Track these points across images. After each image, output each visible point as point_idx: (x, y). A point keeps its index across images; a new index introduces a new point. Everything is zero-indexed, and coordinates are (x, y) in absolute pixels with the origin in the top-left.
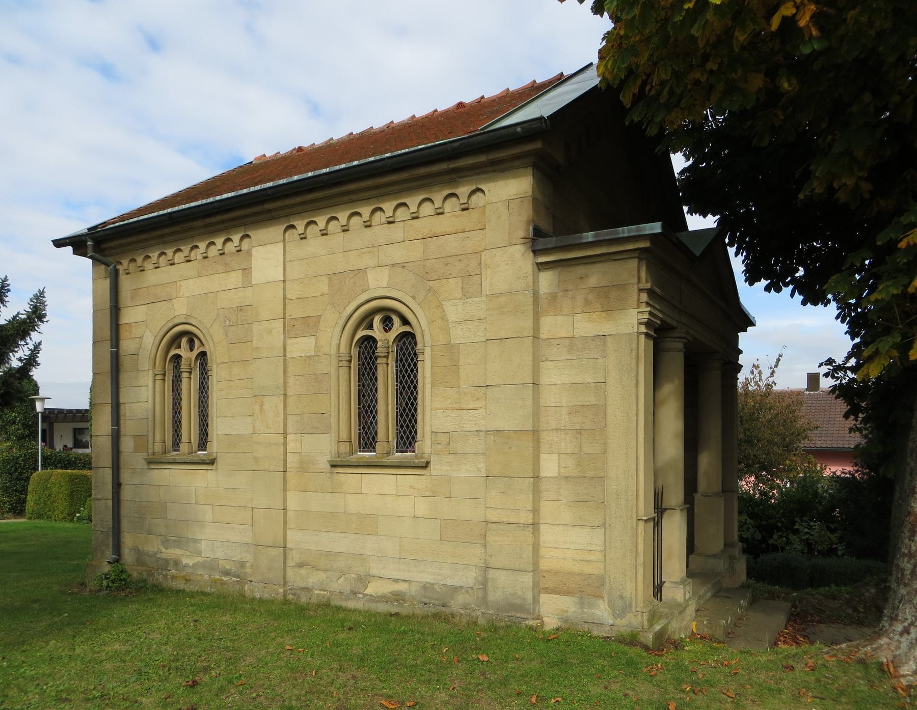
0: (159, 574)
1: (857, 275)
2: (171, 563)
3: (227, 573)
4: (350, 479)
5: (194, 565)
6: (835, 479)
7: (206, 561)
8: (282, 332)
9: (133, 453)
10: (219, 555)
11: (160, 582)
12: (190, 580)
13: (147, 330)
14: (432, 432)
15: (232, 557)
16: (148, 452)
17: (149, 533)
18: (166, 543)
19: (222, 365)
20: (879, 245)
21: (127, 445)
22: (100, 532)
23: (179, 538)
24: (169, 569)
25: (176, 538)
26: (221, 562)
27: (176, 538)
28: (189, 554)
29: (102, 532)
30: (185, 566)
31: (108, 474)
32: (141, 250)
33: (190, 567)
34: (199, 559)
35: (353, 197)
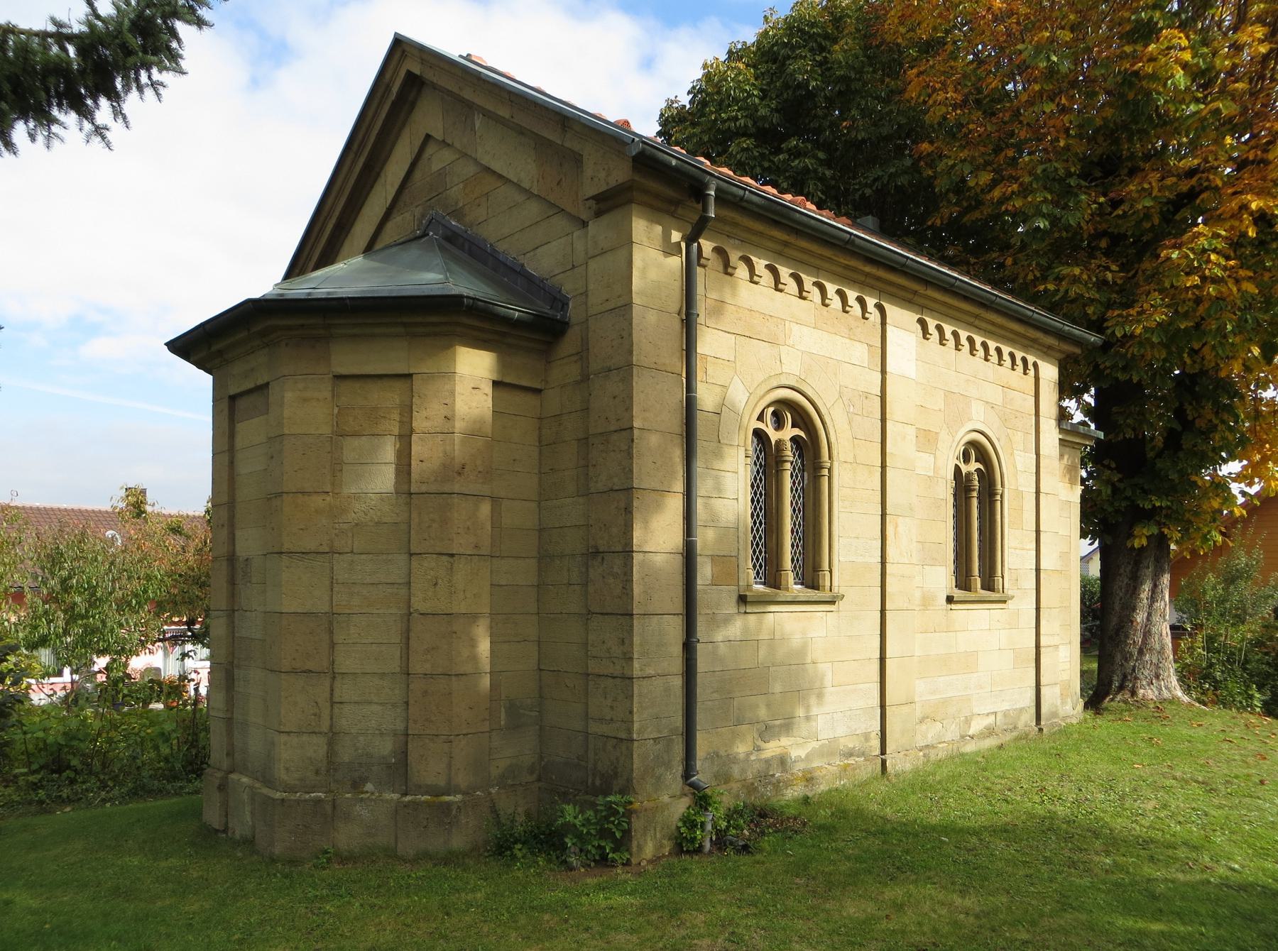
0: (765, 786)
1: (1228, 137)
2: (775, 764)
3: (850, 754)
4: (961, 614)
5: (807, 756)
6: (757, 591)
7: (823, 744)
8: (533, 130)
9: (709, 587)
10: (841, 731)
11: (769, 799)
12: (812, 778)
13: (736, 377)
14: (737, 473)
15: (856, 730)
16: (738, 585)
17: (739, 722)
18: (767, 732)
19: (845, 465)
20: (1224, 138)
21: (705, 572)
22: (652, 741)
23: (787, 721)
24: (771, 773)
25: (782, 721)
26: (842, 740)
27: (782, 721)
28: (800, 740)
29: (654, 739)
30: (795, 761)
31: (673, 629)
32: (737, 242)
33: (802, 760)
34: (815, 745)
35: (951, 312)
